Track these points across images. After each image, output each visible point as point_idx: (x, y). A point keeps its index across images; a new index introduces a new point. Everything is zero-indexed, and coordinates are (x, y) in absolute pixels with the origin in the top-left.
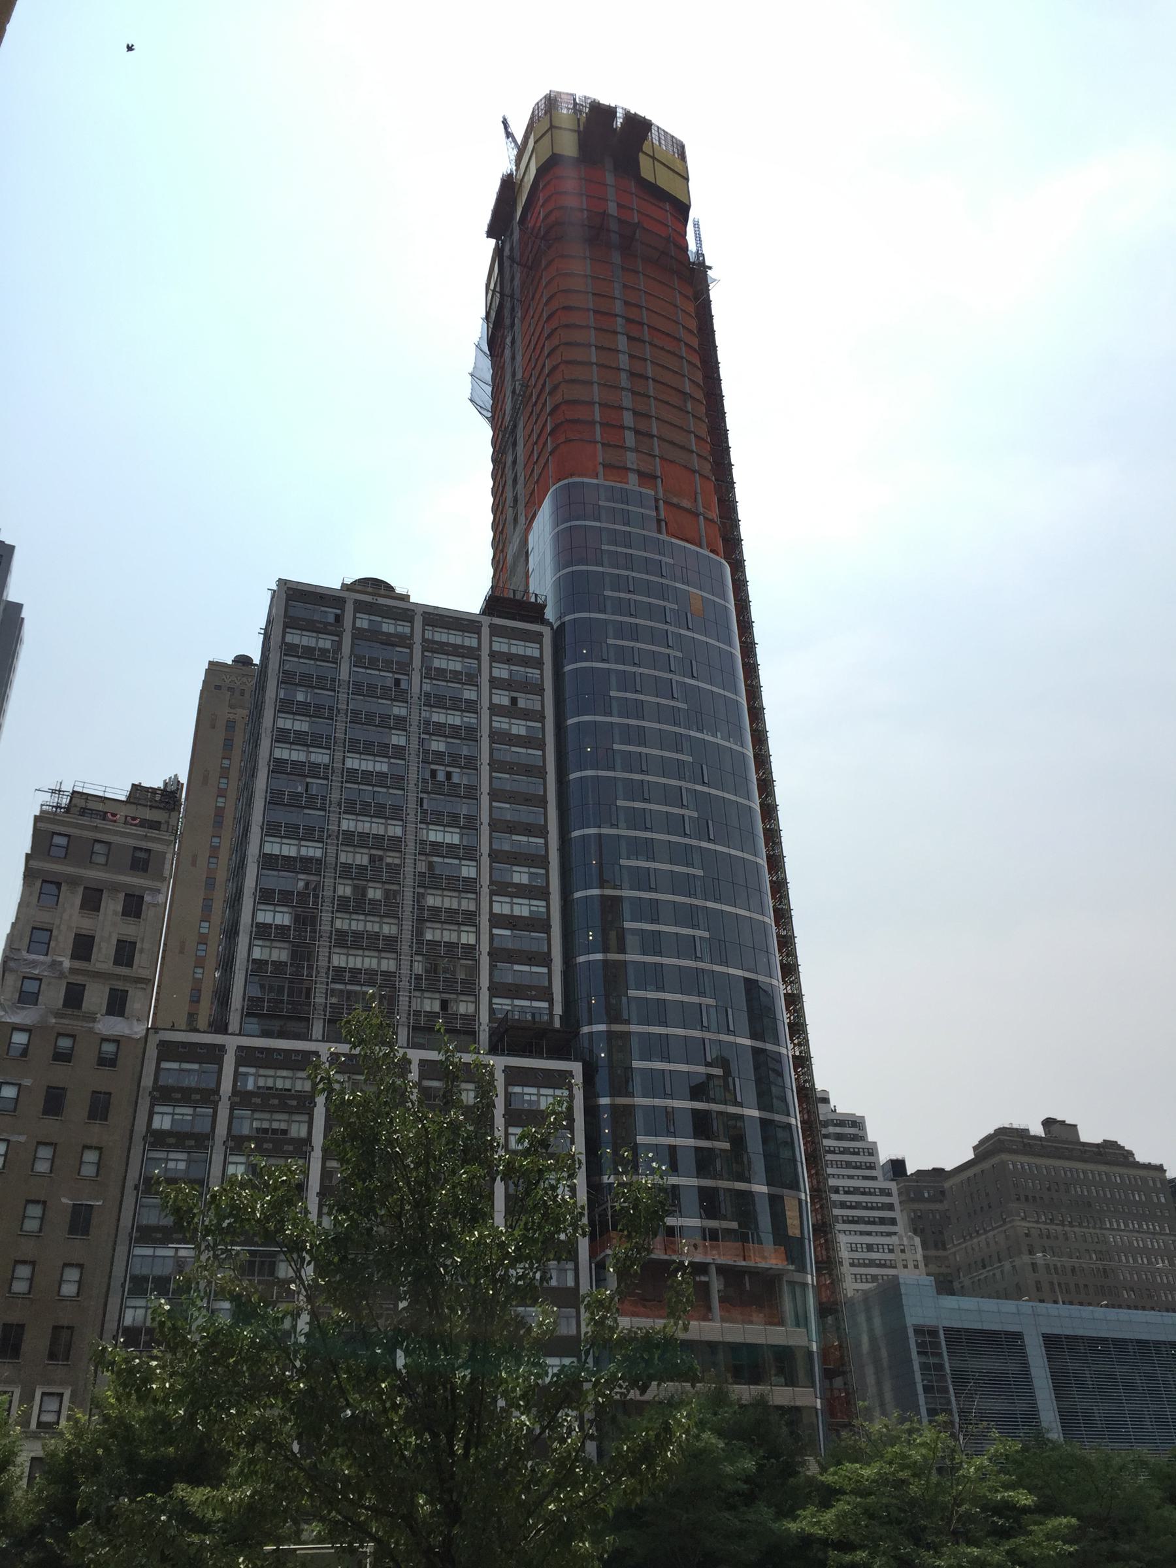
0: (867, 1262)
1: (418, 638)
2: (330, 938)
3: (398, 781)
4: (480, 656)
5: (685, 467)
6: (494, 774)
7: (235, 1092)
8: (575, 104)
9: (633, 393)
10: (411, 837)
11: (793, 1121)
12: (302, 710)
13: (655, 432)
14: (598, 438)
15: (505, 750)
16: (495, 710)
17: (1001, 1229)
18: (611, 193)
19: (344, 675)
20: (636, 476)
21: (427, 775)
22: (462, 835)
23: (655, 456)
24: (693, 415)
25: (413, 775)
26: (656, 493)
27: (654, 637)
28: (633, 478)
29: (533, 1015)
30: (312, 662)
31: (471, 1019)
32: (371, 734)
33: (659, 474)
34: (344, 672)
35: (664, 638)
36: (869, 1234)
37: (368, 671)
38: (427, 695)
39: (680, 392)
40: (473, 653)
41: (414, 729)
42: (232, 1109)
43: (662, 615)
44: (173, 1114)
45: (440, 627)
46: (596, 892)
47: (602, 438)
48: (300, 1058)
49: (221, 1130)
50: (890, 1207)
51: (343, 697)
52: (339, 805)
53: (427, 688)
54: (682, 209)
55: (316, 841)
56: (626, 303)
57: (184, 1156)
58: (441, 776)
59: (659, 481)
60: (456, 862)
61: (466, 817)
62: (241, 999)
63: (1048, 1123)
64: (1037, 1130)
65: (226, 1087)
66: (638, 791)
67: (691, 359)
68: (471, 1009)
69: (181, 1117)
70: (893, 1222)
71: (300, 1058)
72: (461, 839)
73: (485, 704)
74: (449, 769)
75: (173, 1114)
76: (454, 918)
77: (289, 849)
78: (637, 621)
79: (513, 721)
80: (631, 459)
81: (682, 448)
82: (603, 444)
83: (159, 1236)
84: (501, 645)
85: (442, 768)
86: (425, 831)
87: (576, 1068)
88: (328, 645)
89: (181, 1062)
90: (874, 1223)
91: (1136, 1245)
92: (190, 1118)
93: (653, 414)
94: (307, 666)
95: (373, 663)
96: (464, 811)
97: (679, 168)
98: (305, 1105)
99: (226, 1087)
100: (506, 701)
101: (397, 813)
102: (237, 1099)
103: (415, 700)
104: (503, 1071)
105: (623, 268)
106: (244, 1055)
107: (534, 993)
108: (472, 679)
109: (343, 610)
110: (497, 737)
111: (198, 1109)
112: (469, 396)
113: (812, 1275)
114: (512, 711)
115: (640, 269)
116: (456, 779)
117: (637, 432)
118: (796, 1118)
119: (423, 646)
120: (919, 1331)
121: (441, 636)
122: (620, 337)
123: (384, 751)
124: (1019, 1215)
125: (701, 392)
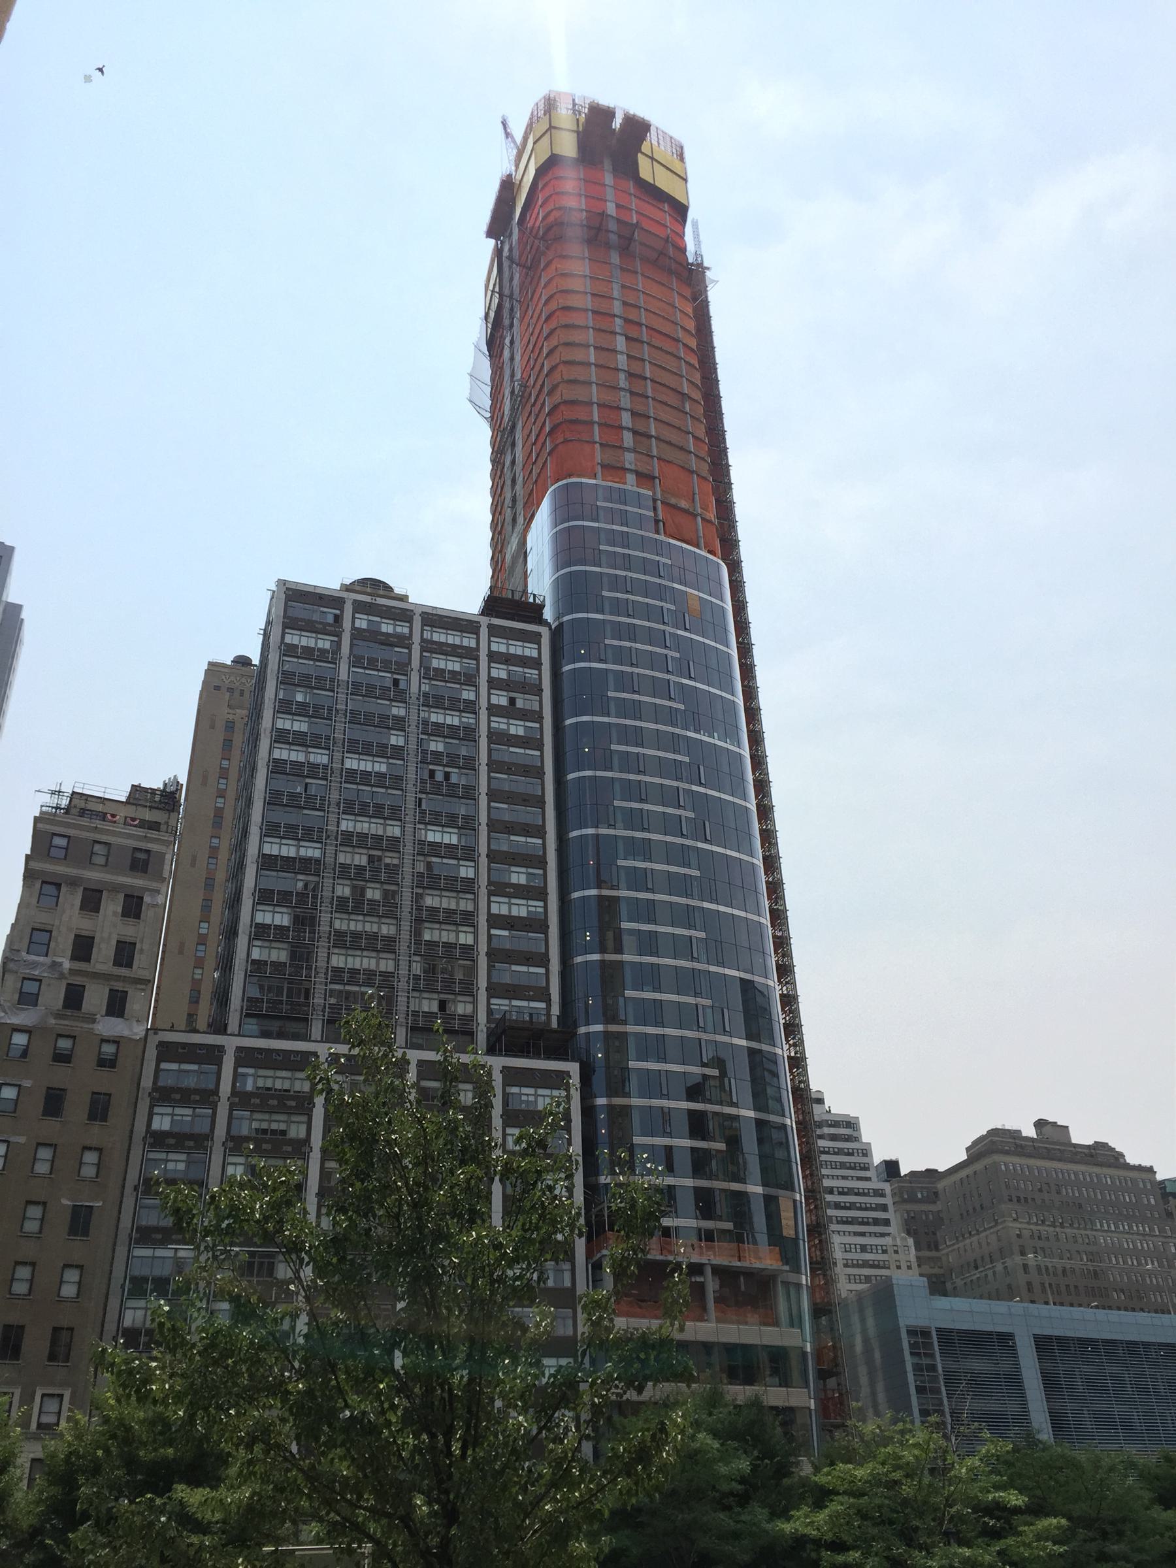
1: (416, 639)
2: (329, 938)
3: (397, 781)
4: (479, 656)
7: (234, 1093)
8: (574, 105)
9: (632, 393)
10: (409, 837)
11: (788, 1122)
12: (301, 710)
14: (597, 439)
16: (493, 710)
17: (992, 1230)
18: (610, 194)
20: (634, 476)
21: (426, 776)
25: (411, 775)
26: (654, 493)
28: (631, 478)
30: (311, 663)
31: (469, 1019)
32: (371, 735)
35: (660, 639)
36: (863, 1234)
37: (367, 672)
40: (471, 654)
41: (413, 729)
42: (231, 1110)
44: (173, 1115)
45: (439, 628)
46: (593, 892)
49: (220, 1132)
50: (884, 1208)
52: (338, 804)
53: (425, 688)
54: (680, 210)
56: (625, 304)
57: (183, 1157)
58: (439, 777)
60: (454, 862)
63: (1040, 1124)
64: (1030, 1132)
65: (225, 1088)
68: (469, 1009)
69: (179, 1118)
70: (887, 1222)
72: (459, 840)
73: (484, 704)
74: (447, 769)
75: (173, 1115)
76: (452, 918)
77: (288, 850)
79: (511, 721)
80: (629, 459)
81: (681, 448)
83: (159, 1236)
84: (500, 646)
85: (441, 768)
88: (327, 645)
89: (180, 1063)
90: (867, 1224)
92: (189, 1118)
95: (372, 664)
99: (225, 1088)
100: (504, 702)
101: (395, 814)
102: (237, 1100)
103: (414, 700)
104: (501, 1072)
107: (531, 993)
110: (495, 737)
112: (467, 394)
113: (807, 1276)
114: (511, 711)
116: (454, 779)
117: (635, 433)
118: (791, 1119)
119: (422, 647)
120: (912, 1332)
121: (440, 637)
123: (383, 751)
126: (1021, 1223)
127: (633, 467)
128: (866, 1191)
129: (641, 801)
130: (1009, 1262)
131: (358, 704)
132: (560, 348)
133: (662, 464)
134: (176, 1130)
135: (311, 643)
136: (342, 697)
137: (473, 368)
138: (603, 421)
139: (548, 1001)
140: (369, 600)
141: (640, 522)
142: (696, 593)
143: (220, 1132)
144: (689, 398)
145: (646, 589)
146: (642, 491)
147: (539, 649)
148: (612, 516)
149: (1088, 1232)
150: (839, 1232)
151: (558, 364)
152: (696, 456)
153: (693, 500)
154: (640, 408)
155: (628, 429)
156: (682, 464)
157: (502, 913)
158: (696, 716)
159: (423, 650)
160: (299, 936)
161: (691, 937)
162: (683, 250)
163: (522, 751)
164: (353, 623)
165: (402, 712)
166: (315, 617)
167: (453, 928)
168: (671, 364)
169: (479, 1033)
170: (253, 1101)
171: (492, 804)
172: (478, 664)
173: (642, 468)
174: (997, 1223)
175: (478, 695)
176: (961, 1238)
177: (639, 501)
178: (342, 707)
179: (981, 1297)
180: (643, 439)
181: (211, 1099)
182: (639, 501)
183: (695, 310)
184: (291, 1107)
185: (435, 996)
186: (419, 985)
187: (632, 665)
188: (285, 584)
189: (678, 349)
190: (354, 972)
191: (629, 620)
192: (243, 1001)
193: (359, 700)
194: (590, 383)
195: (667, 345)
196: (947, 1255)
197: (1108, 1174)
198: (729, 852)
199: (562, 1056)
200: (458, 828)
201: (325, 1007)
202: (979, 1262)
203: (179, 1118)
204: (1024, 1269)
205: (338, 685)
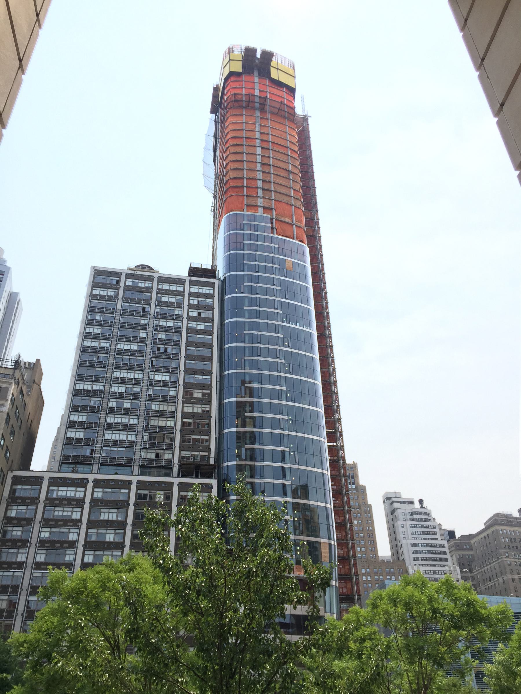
0: (433, 579)
1: (155, 288)
2: (104, 426)
3: (141, 353)
4: (184, 295)
5: (287, 204)
6: (188, 348)
7: (47, 498)
9: (263, 172)
12: (98, 324)
15: (194, 337)
17: (496, 562)
18: (257, 86)
19: (119, 307)
20: (262, 209)
22: (170, 376)
23: (272, 200)
25: (149, 350)
26: (272, 215)
27: (267, 281)
28: (261, 210)
29: (194, 458)
30: (104, 302)
31: (170, 461)
32: (131, 333)
33: (274, 207)
35: (272, 281)
36: (435, 566)
37: (131, 304)
38: (158, 313)
39: (287, 170)
40: (181, 294)
41: (151, 329)
42: (45, 507)
44: (17, 509)
45: (166, 283)
46: (234, 399)
48: (79, 482)
49: (39, 517)
50: (445, 553)
52: (113, 365)
53: (158, 310)
54: (292, 91)
56: (261, 133)
57: (21, 529)
58: (162, 350)
59: (274, 210)
60: (167, 389)
65: (43, 496)
66: (254, 352)
67: (294, 156)
69: (20, 511)
70: (446, 560)
71: (79, 482)
73: (185, 316)
74: (166, 347)
75: (17, 509)
76: (164, 415)
77: (88, 387)
79: (198, 323)
80: (260, 202)
81: (287, 195)
83: (6, 566)
84: (195, 289)
85: (163, 346)
86: (153, 375)
87: (214, 482)
89: (22, 485)
90: (436, 560)
92: (25, 511)
94: (102, 303)
95: (133, 301)
96: (173, 365)
98: (80, 504)
99: (43, 496)
100: (195, 314)
101: (139, 368)
102: (48, 502)
103: (152, 316)
104: (178, 485)
107: (201, 448)
108: (179, 305)
109: (120, 278)
110: (189, 331)
111: (29, 507)
112: (203, 184)
113: (336, 581)
114: (199, 319)
116: (169, 351)
117: (264, 189)
119: (157, 292)
121: (166, 287)
122: (258, 148)
123: (136, 340)
124: (505, 555)
125: (298, 170)
126: (510, 558)
127: (262, 205)
128: (435, 545)
129: (258, 356)
132: (230, 156)
133: (277, 202)
134: (18, 516)
135: (105, 293)
136: (118, 317)
138: (248, 186)
139: (209, 452)
141: (264, 229)
142: (291, 259)
143: (39, 517)
145: (265, 259)
146: (265, 215)
148: (250, 227)
152: (294, 198)
153: (292, 218)
154: (266, 179)
155: (260, 188)
156: (286, 202)
157: (189, 411)
158: (288, 316)
159: (158, 293)
161: (280, 418)
164: (125, 283)
165: (146, 322)
166: (108, 282)
167: (165, 419)
169: (174, 468)
170: (55, 502)
172: (184, 298)
173: (266, 205)
174: (498, 559)
177: (264, 220)
179: (493, 595)
181: (36, 501)
182: (264, 220)
183: (299, 134)
185: (154, 451)
187: (257, 294)
188: (94, 268)
189: (287, 151)
190: (115, 441)
192: (61, 456)
194: (243, 169)
195: (281, 150)
196: (477, 574)
198: (302, 378)
199: (210, 477)
201: (100, 458)
203: (20, 511)
205: (116, 311)
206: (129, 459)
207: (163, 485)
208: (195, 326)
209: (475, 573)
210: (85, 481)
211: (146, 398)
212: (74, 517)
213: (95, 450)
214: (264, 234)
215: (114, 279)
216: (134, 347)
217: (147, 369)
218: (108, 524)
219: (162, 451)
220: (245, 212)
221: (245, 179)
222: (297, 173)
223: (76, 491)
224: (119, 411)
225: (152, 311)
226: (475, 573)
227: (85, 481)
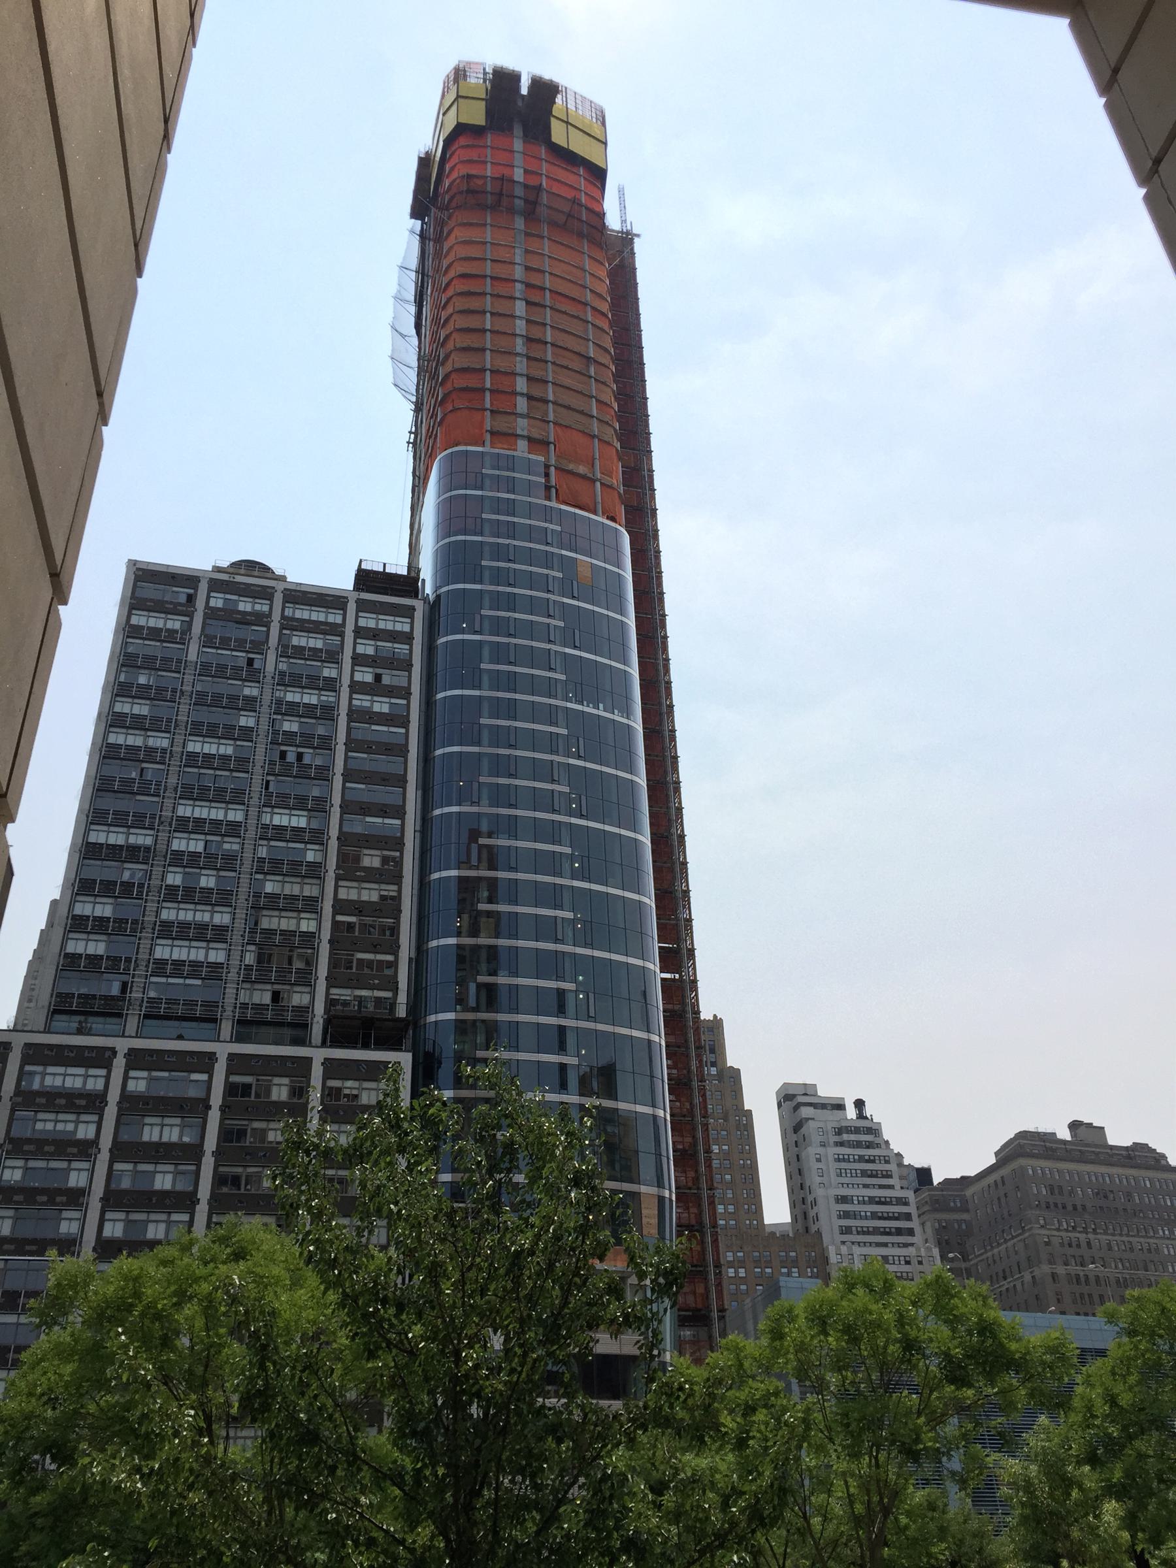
1: (276, 616)
3: (242, 763)
5: (583, 432)
6: (350, 754)
7: (18, 1092)
9: (529, 358)
10: (252, 822)
11: (661, 1113)
12: (143, 693)
13: (551, 397)
14: (488, 405)
16: (356, 687)
17: (1019, 1238)
18: (518, 160)
19: (192, 656)
22: (309, 818)
24: (595, 380)
26: (547, 459)
27: (533, 605)
28: (522, 445)
30: (158, 644)
31: (304, 1011)
32: (218, 716)
33: (552, 439)
34: (193, 652)
36: (885, 1245)
37: (219, 651)
40: (337, 630)
41: (265, 709)
43: (544, 584)
47: (492, 404)
48: (94, 1055)
50: (908, 1217)
51: (189, 678)
52: (176, 789)
53: (283, 666)
54: (598, 175)
55: (147, 828)
56: (527, 268)
58: (291, 758)
60: (302, 846)
61: (315, 799)
62: (48, 995)
63: (1075, 1126)
64: (1064, 1134)
67: (598, 323)
68: (305, 1000)
70: (911, 1232)
71: (94, 1055)
72: (309, 823)
73: (346, 681)
76: (291, 904)
78: (516, 590)
79: (375, 698)
80: (522, 427)
81: (582, 412)
82: (492, 411)
85: (293, 749)
87: (405, 1059)
88: (177, 626)
91: (1166, 1253)
93: (550, 379)
95: (225, 643)
96: (316, 792)
97: (597, 131)
100: (369, 678)
101: (237, 797)
102: (20, 1099)
103: (268, 679)
104: (322, 1064)
105: (527, 234)
106: (31, 1052)
107: (376, 982)
108: (333, 657)
112: (392, 380)
114: (376, 688)
115: (546, 234)
117: (530, 398)
118: (665, 1110)
119: (281, 624)
121: (303, 613)
122: (518, 303)
123: (229, 733)
127: (525, 433)
128: (888, 1200)
130: (1037, 1272)
131: (206, 685)
133: (559, 430)
135: (160, 624)
137: (393, 350)
140: (227, 579)
141: (529, 488)
142: (589, 560)
144: (595, 361)
147: (412, 624)
149: (1125, 1239)
150: (859, 1243)
151: (451, 333)
155: (522, 394)
159: (282, 627)
160: (120, 926)
161: (556, 917)
162: (601, 215)
163: (385, 729)
164: (207, 602)
168: (575, 327)
169: (314, 1025)
170: (58, 1101)
171: (348, 785)
173: (535, 434)
175: (340, 674)
176: (989, 1248)
177: (529, 468)
178: (189, 688)
180: (540, 405)
182: (529, 468)
183: (612, 274)
184: (80, 1107)
185: (269, 987)
186: (249, 977)
188: (135, 565)
190: (178, 964)
191: (509, 589)
192: (52, 996)
193: (209, 681)
196: (977, 1264)
197: (1146, 1177)
200: (309, 810)
201: (143, 1001)
202: (1008, 1273)
204: (1053, 1278)
206: (211, 1005)
207: (289, 1064)
208: (367, 704)
209: (972, 1263)
210: (108, 1054)
211: (253, 866)
212: (80, 1135)
213: (132, 982)
214: (529, 499)
215: (182, 593)
216: (227, 749)
217: (255, 801)
218: (161, 1152)
219: (288, 987)
220: (487, 449)
221: (488, 373)
222: (607, 364)
223: (86, 1076)
224: (189, 895)
225: (270, 668)
226: (972, 1263)
227: (108, 1054)
